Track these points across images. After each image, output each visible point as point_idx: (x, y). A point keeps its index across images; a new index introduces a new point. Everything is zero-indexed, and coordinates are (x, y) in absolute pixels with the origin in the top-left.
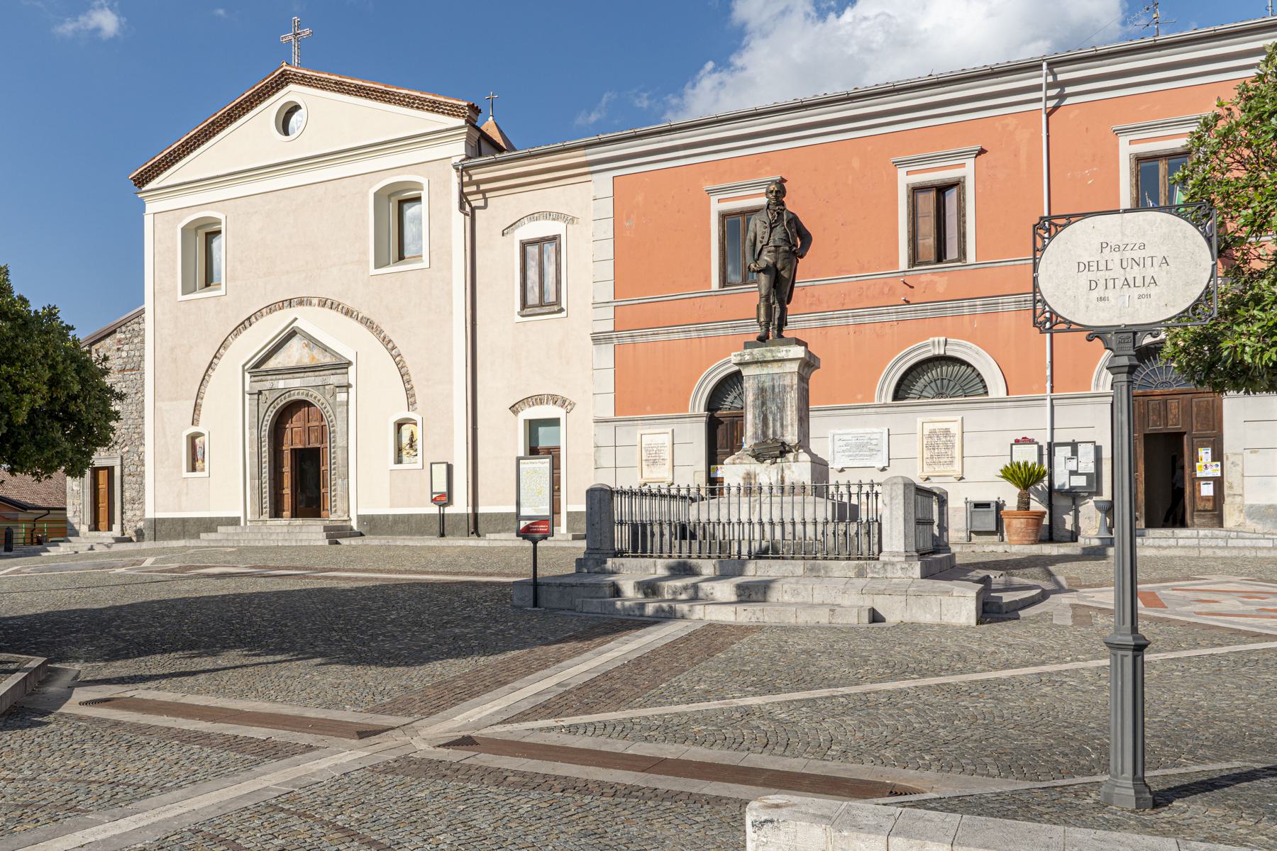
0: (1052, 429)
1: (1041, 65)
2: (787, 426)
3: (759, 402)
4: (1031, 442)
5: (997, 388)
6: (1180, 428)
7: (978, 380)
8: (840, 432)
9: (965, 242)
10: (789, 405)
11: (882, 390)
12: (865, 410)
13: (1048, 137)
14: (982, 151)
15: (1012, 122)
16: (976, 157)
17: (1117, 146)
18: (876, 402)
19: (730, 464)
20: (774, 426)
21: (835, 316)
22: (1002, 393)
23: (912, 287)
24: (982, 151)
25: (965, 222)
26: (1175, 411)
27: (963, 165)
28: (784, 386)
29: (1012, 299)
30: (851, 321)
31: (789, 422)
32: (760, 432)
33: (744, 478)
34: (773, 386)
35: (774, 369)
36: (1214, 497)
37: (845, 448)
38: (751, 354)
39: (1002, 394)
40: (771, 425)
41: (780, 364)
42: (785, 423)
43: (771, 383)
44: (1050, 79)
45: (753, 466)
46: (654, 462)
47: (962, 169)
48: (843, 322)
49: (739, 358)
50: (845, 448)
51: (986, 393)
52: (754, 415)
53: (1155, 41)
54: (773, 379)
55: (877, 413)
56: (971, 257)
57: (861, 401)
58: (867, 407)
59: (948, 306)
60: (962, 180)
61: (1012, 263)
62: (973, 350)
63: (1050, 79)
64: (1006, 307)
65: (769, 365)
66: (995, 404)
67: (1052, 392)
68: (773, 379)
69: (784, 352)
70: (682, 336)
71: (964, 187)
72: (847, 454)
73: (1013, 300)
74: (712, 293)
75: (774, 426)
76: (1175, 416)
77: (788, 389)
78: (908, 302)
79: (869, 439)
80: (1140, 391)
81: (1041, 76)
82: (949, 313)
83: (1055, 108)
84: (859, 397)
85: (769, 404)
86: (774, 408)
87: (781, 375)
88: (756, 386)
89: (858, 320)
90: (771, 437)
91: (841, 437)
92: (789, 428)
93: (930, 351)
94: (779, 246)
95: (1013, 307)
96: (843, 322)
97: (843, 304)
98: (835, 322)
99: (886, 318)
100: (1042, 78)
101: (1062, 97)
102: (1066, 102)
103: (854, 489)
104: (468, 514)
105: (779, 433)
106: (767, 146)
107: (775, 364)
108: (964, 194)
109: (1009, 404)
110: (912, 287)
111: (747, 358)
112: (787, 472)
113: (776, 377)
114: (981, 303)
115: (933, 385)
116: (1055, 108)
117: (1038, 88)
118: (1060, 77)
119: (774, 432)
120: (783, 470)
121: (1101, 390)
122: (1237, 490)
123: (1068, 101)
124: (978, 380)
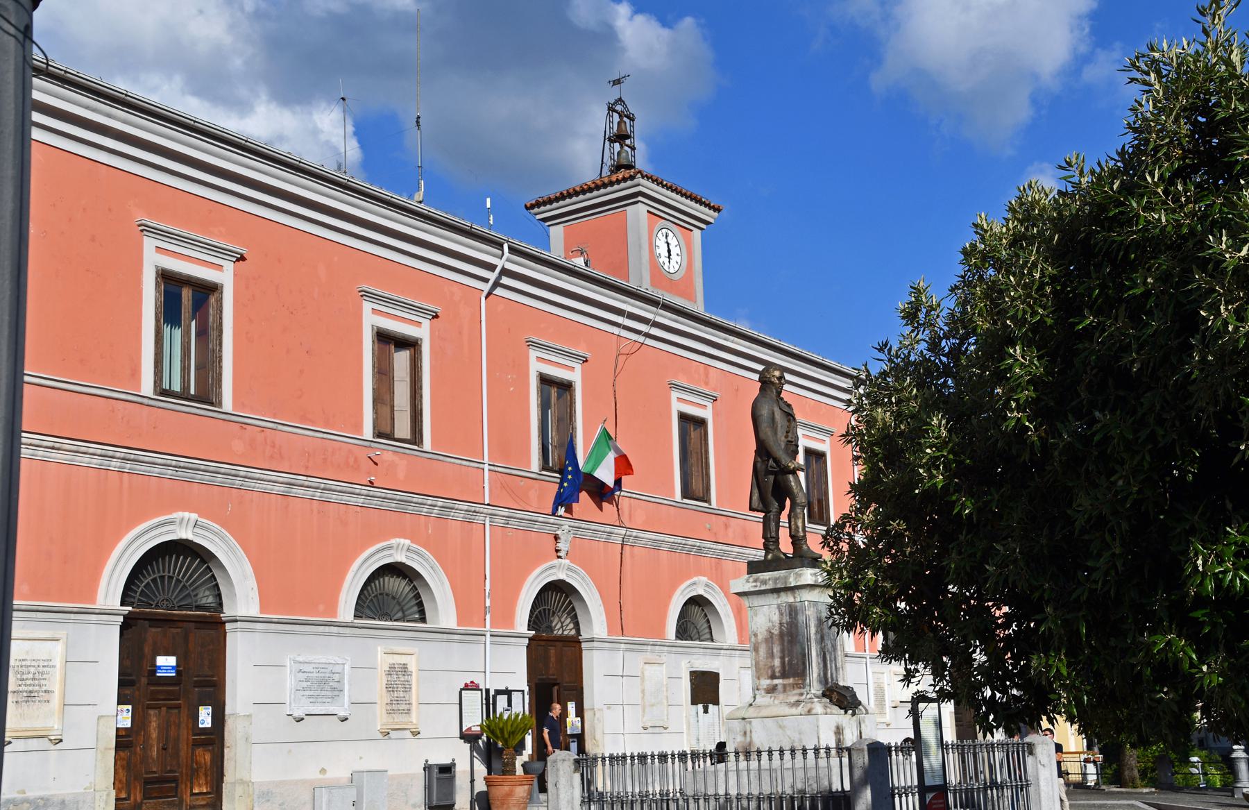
3: (819, 636)
4: (476, 688)
5: (444, 611)
7: (414, 602)
8: (300, 659)
15: (455, 288)
20: (831, 667)
21: (306, 483)
23: (376, 464)
37: (305, 684)
46: (30, 696)
47: (702, 410)
50: (305, 684)
51: (423, 620)
56: (427, 444)
59: (415, 500)
61: (459, 461)
62: (429, 563)
70: (96, 461)
73: (466, 508)
74: (139, 399)
75: (831, 667)
78: (371, 484)
82: (410, 509)
93: (173, 532)
96: (309, 493)
97: (307, 468)
99: (353, 500)
110: (376, 464)
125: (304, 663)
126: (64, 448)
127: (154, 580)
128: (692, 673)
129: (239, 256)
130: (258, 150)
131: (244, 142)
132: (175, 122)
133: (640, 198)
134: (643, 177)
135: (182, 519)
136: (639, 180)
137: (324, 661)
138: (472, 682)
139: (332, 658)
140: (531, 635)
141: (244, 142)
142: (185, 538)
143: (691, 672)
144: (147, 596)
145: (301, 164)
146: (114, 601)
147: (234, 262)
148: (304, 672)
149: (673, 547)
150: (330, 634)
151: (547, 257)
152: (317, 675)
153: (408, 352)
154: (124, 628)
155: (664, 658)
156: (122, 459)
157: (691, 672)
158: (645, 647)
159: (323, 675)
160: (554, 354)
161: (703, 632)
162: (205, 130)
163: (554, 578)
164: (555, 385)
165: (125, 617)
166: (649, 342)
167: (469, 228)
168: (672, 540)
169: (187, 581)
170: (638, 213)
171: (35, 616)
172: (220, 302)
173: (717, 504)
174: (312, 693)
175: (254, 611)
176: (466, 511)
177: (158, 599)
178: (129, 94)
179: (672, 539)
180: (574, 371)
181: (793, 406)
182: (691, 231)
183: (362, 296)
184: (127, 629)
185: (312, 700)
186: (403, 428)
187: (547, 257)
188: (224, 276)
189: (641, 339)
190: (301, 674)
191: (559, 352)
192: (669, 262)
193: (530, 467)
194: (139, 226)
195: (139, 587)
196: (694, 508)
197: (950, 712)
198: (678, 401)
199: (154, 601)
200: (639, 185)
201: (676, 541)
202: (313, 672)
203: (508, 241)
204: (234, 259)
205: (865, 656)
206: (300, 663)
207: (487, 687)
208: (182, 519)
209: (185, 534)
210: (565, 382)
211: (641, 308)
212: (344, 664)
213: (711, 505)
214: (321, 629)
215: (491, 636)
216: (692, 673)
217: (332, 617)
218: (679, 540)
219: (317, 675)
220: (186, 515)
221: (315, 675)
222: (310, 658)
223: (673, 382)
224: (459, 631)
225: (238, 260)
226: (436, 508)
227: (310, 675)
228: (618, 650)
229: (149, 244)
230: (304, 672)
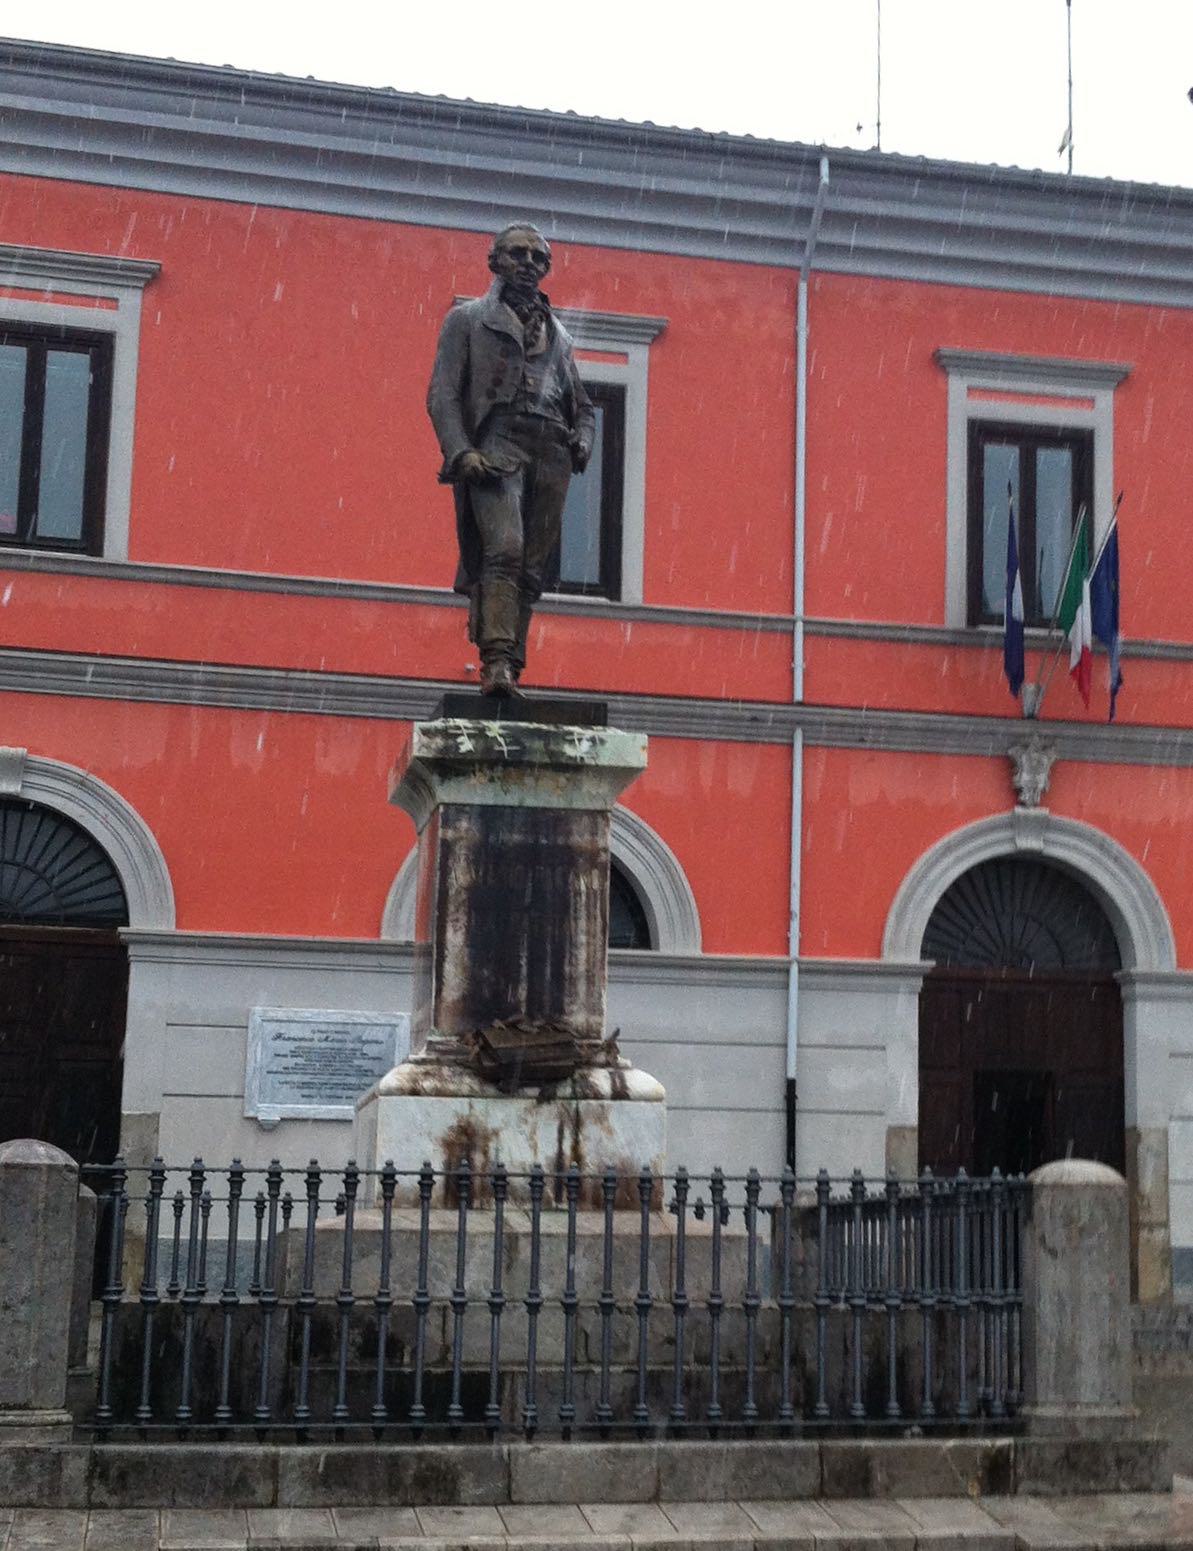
1: (816, 164)
8: (281, 1014)
19: (401, 1092)
31: (582, 968)
33: (448, 1145)
36: (308, 1229)
45: (479, 1105)
49: (439, 742)
50: (291, 1062)
55: (381, 970)
56: (117, 543)
69: (585, 746)
72: (296, 1078)
79: (359, 1040)
91: (283, 1029)
103: (735, 1194)
104: (671, 1237)
109: (705, 975)
112: (591, 1130)
115: (41, 888)
120: (577, 1124)
122: (1156, 1215)
129: (656, 332)
137: (339, 1018)
139: (361, 1015)
140: (929, 971)
146: (913, 958)
149: (210, 695)
152: (324, 1045)
159: (337, 1045)
171: (167, 954)
174: (307, 1079)
175: (167, 926)
180: (116, 308)
185: (306, 1092)
186: (59, 516)
190: (279, 1042)
196: (433, 599)
197: (895, 1133)
202: (312, 1040)
207: (792, 1074)
215: (800, 971)
219: (324, 1045)
222: (307, 1013)
227: (303, 1044)
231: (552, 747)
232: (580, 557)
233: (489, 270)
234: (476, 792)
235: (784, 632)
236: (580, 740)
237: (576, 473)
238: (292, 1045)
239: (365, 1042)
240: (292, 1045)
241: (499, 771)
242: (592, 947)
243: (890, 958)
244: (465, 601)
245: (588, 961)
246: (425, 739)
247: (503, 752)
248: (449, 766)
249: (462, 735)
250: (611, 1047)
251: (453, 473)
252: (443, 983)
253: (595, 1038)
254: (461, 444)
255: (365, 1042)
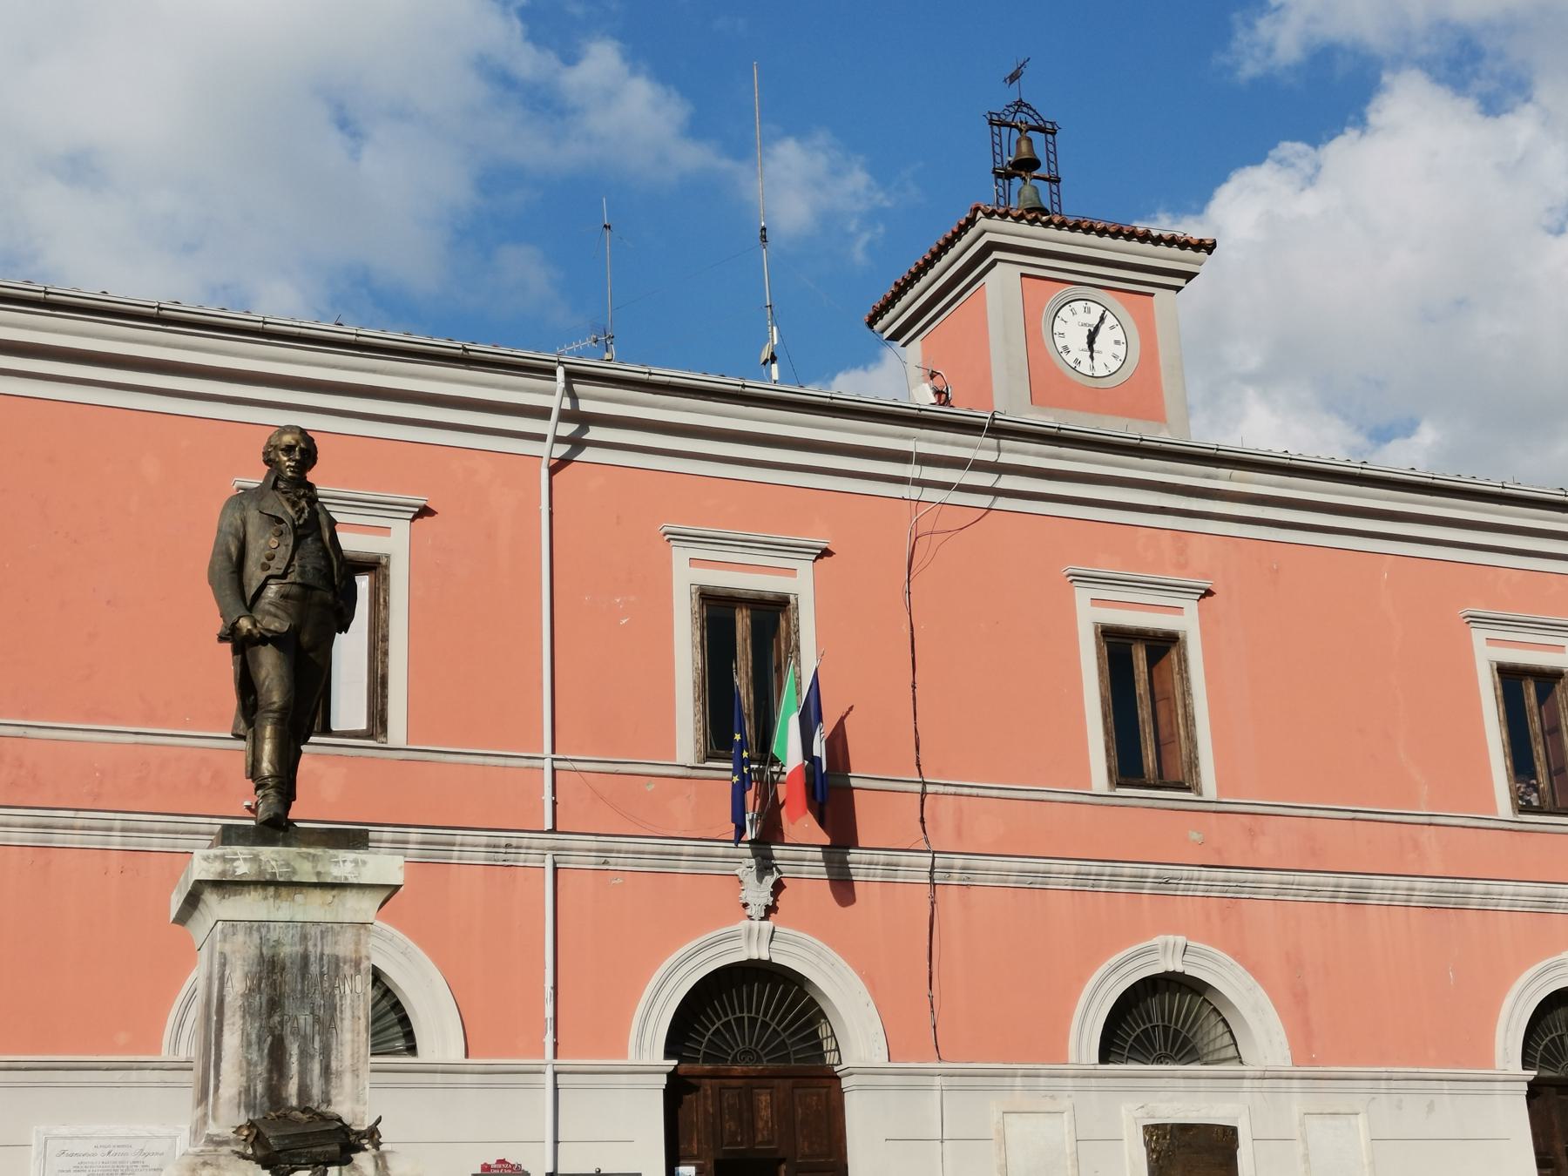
0: (556, 1142)
1: (553, 372)
2: (339, 1074)
6: (776, 1151)
7: (393, 1017)
9: (385, 696)
10: (348, 1014)
11: (181, 1025)
12: (134, 1075)
13: (551, 513)
14: (425, 512)
16: (412, 520)
17: (669, 563)
18: (165, 1054)
20: (304, 1072)
21: (79, 823)
22: (453, 1052)
24: (425, 512)
25: (386, 653)
26: (765, 1113)
27: (386, 530)
28: (336, 962)
29: (482, 838)
30: (116, 841)
31: (347, 1062)
32: (260, 1088)
34: (305, 958)
35: (311, 908)
38: (255, 859)
39: (455, 1054)
40: (294, 1067)
41: (329, 896)
42: (334, 1065)
43: (299, 949)
44: (567, 404)
48: (95, 840)
51: (412, 1049)
52: (245, 1035)
53: (744, 386)
54: (304, 938)
55: (165, 1085)
56: (397, 730)
57: (124, 1050)
58: (140, 1067)
60: (383, 561)
61: (480, 760)
63: (567, 404)
64: (468, 857)
65: (299, 898)
66: (439, 1078)
67: (555, 1056)
68: (304, 938)
69: (349, 866)
71: (386, 578)
75: (304, 1072)
76: (767, 1122)
77: (347, 969)
80: (708, 1067)
81: (553, 393)
83: (564, 462)
84: (122, 1038)
85: (290, 1006)
86: (304, 1019)
87: (328, 929)
88: (253, 952)
89: (135, 842)
90: (294, 1102)
92: (348, 1079)
93: (738, 949)
94: (313, 588)
95: (480, 857)
96: (95, 840)
98: (74, 839)
100: (553, 396)
101: (577, 443)
102: (583, 456)
105: (316, 1091)
106: (956, 264)
107: (317, 896)
108: (387, 591)
109: (467, 1078)
111: (243, 869)
113: (314, 931)
114: (420, 837)
116: (564, 462)
117: (543, 413)
118: (586, 406)
119: (303, 1091)
121: (646, 1060)
123: (588, 454)
124: (393, 1017)
125: (71, 1138)
126: (574, 847)
127: (727, 1025)
128: (1151, 1130)
130: (1003, 425)
131: (828, 400)
132: (238, 329)
133: (996, 255)
134: (989, 215)
135: (1166, 944)
136: (983, 223)
138: (502, 1162)
140: (1532, 1078)
141: (828, 400)
142: (756, 958)
143: (1145, 1127)
144: (1551, 1053)
145: (834, 401)
147: (1198, 600)
148: (72, 1155)
150: (142, 1085)
151: (668, 379)
152: (107, 1158)
153: (367, 577)
154: (1531, 1096)
155: (1065, 1103)
156: (1075, 874)
157: (1145, 1127)
158: (1007, 1081)
160: (738, 549)
161: (1218, 1044)
162: (689, 385)
163: (1158, 969)
164: (743, 604)
165: (1530, 1084)
166: (1003, 503)
167: (1138, 441)
168: (1074, 869)
169: (1176, 1024)
170: (1002, 281)
172: (1183, 660)
173: (1220, 788)
176: (487, 846)
177: (736, 1051)
178: (1220, 448)
179: (1073, 867)
180: (1564, 652)
181: (261, 458)
182: (1152, 295)
183: (1468, 623)
184: (1534, 1098)
187: (1158, 444)
188: (1185, 620)
189: (984, 501)
190: (63, 1158)
191: (747, 544)
192: (1092, 357)
193: (1089, 786)
194: (665, 534)
195: (1127, 1041)
198: (1488, 644)
199: (729, 1055)
200: (984, 232)
201: (1084, 870)
203: (561, 363)
204: (814, 557)
205: (542, 1068)
206: (65, 1138)
208: (1166, 944)
209: (1173, 964)
210: (771, 597)
211: (954, 444)
212: (175, 1137)
213: (1200, 794)
214: (118, 1075)
216: (1151, 1130)
217: (147, 1053)
218: (1094, 868)
219: (107, 1158)
220: (1171, 938)
221: (99, 1158)
223: (1070, 571)
224: (469, 1068)
225: (1203, 596)
226: (1182, 882)
228: (929, 1088)
229: (1479, 636)
230: (72, 1155)
231: (319, 869)
232: (348, 708)
233: (263, 463)
234: (250, 906)
235: (372, 734)
236: (344, 861)
237: (340, 633)
238: (75, 1161)
239: (146, 1155)
240: (75, 1161)
241: (271, 890)
242: (356, 1045)
243: (632, 1058)
244: (241, 744)
245: (352, 1055)
246: (205, 864)
247: (275, 873)
248: (226, 885)
249: (238, 859)
250: (373, 1134)
251: (231, 635)
252: (219, 1081)
253: (361, 1125)
254: (236, 609)
255: (146, 1155)
